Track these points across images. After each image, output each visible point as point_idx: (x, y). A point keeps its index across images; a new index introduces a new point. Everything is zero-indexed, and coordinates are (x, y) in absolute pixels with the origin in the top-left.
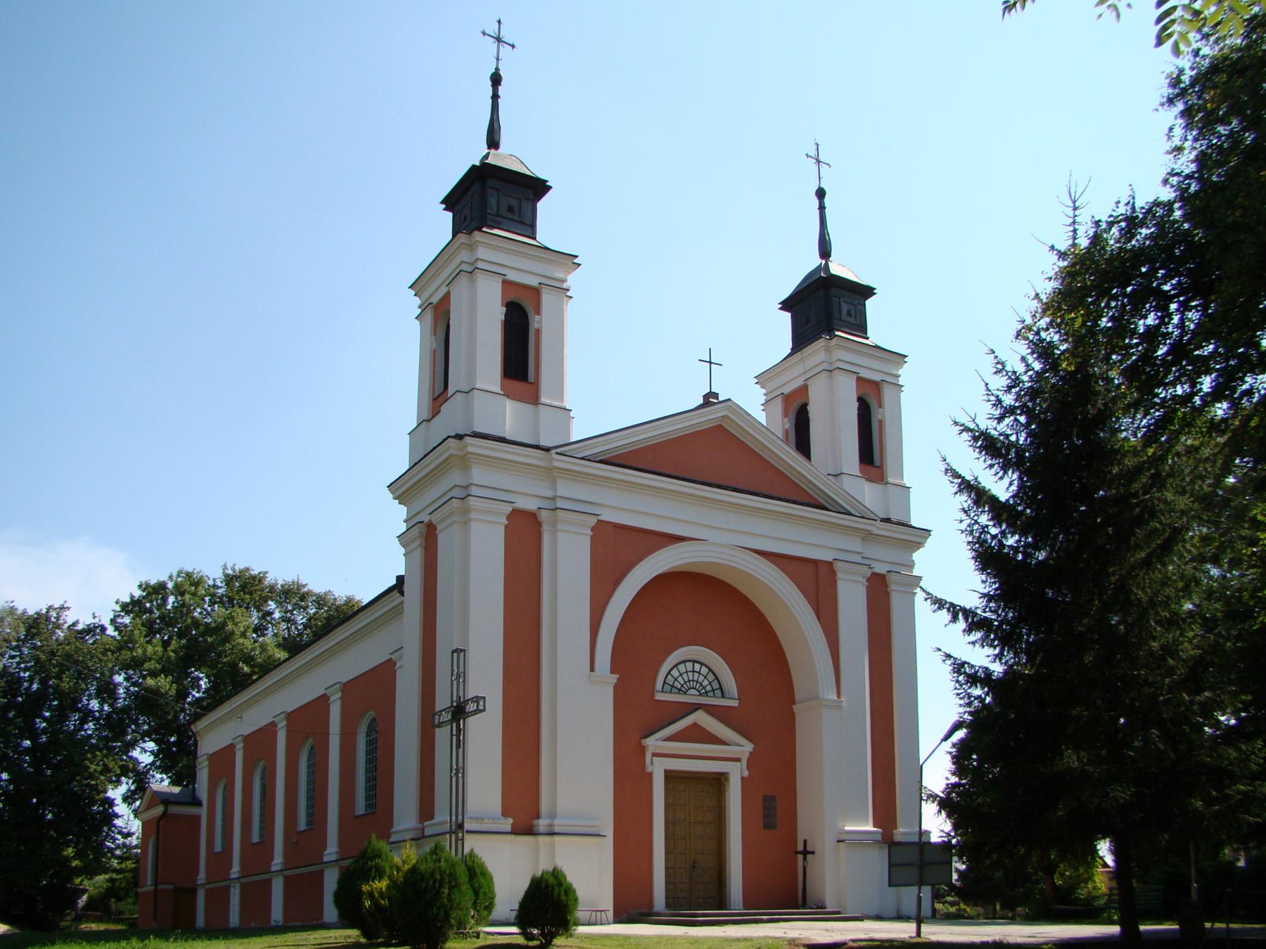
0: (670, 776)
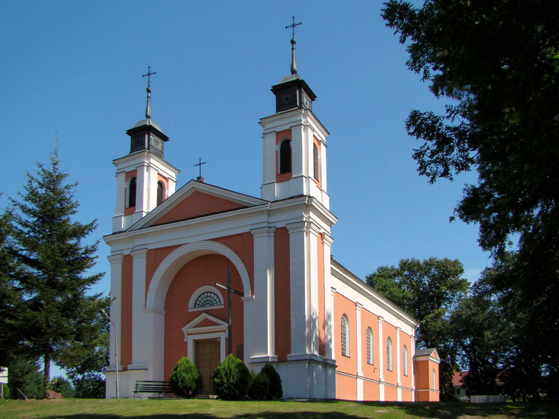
0: (197, 343)
